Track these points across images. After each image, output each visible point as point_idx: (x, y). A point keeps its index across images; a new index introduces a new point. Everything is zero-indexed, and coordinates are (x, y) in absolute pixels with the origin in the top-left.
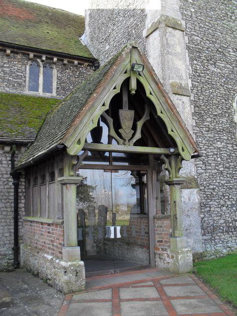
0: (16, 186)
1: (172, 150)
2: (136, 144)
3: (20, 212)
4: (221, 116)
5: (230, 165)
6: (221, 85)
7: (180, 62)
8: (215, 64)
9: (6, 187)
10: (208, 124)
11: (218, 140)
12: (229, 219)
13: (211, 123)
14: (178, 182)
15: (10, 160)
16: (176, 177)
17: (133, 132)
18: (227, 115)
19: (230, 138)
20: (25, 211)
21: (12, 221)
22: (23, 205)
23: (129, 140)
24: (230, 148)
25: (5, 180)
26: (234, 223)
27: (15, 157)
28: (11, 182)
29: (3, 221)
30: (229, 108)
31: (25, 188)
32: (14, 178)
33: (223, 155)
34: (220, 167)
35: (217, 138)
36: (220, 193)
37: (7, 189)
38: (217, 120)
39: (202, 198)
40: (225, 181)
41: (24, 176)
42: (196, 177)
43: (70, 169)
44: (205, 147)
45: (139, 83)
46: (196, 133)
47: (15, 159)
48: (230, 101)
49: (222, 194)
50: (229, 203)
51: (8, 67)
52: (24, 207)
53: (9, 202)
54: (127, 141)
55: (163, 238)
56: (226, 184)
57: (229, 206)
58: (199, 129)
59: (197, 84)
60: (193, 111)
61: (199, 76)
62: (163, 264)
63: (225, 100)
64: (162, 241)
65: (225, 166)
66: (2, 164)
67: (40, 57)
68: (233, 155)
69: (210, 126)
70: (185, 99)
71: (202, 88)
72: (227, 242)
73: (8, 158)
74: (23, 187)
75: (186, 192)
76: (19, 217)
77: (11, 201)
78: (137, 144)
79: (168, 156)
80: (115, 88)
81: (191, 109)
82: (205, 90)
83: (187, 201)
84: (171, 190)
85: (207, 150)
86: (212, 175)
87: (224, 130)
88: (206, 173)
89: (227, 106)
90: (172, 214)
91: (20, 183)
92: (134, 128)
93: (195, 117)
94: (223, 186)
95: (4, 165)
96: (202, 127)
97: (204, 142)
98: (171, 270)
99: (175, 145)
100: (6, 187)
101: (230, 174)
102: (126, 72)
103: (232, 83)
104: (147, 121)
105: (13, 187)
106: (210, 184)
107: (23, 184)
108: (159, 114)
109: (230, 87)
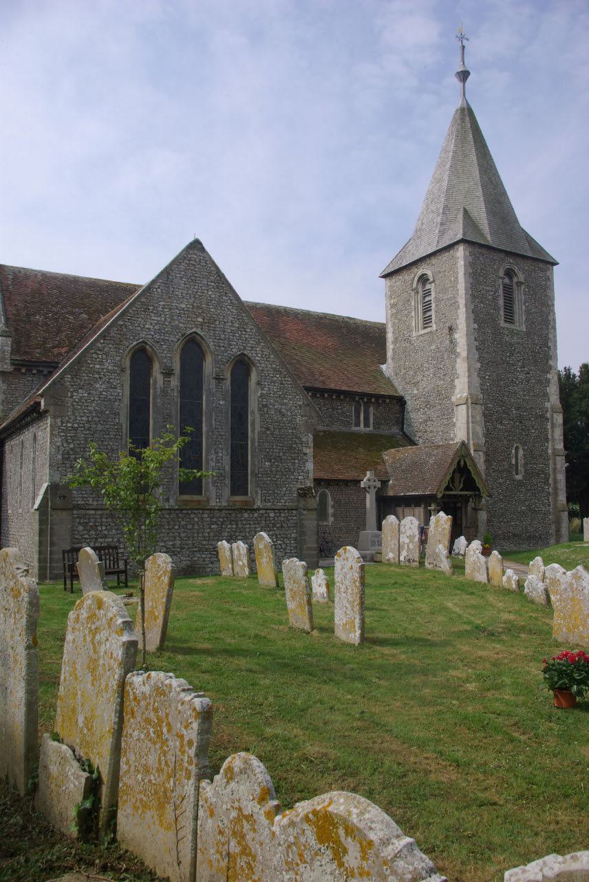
1: (477, 493)
7: (479, 427)
8: (501, 422)
45: (465, 462)
51: (340, 409)
61: (490, 433)
67: (362, 399)
70: (481, 453)
99: (479, 490)
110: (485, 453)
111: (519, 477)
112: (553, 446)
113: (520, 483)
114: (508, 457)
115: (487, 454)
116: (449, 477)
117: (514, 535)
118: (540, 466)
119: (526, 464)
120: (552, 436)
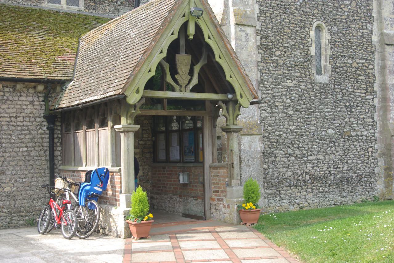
0: (52, 131)
1: (230, 96)
2: (193, 90)
3: (56, 161)
4: (294, 47)
5: (302, 108)
6: (296, 9)
9: (40, 131)
10: (276, 58)
11: (288, 77)
12: (298, 171)
13: (281, 57)
14: (235, 130)
15: (43, 101)
16: (234, 125)
17: (189, 77)
18: (301, 46)
19: (303, 75)
20: (62, 160)
21: (48, 171)
22: (59, 153)
23: (186, 86)
24: (303, 87)
25: (37, 124)
26: (304, 175)
27: (49, 97)
28: (45, 126)
29: (37, 171)
30: (305, 38)
31: (61, 133)
32: (48, 122)
33: (293, 95)
34: (289, 109)
35: (287, 75)
36: (288, 141)
37: (41, 134)
38: (288, 53)
39: (266, 146)
40: (294, 127)
41: (59, 120)
42: (259, 122)
43: (128, 117)
44: (272, 86)
45: (198, 28)
46: (261, 70)
47: (50, 99)
48: (307, 29)
49: (290, 142)
50: (298, 152)
52: (60, 156)
53: (42, 149)
54: (183, 87)
55: (219, 188)
56: (296, 130)
57: (299, 156)
58: (264, 65)
59: (265, 9)
60: (259, 43)
62: (219, 215)
63: (301, 28)
64: (217, 192)
65: (295, 109)
66: (34, 105)
68: (307, 95)
69: (279, 61)
70: (249, 30)
71: (271, 14)
72: (295, 198)
73: (40, 98)
74: (59, 132)
75: (246, 140)
76: (55, 167)
77: (45, 148)
78: (193, 90)
79: (226, 102)
80: (172, 34)
81: (256, 41)
82: (276, 16)
83: (248, 149)
84: (228, 138)
85: (274, 90)
86: (279, 120)
87: (296, 66)
88: (271, 117)
89: (303, 36)
90: (229, 163)
91: (55, 127)
92: (191, 73)
93: (260, 51)
94: (293, 133)
95: (35, 107)
96: (269, 63)
97: (270, 80)
98: (226, 220)
99: (233, 92)
100: (40, 131)
101: (301, 118)
102: (184, 16)
103: (311, 5)
104: (205, 65)
105: (47, 132)
106: (276, 130)
107: (59, 128)
108: (217, 59)
109: (308, 10)
110: (258, 32)
111: (323, 79)
112: (380, 29)
113: (324, 90)
114: (303, 43)
115: (262, 35)
116: (158, 58)
117: (314, 178)
118: (358, 61)
119: (333, 58)
120: (379, 13)
